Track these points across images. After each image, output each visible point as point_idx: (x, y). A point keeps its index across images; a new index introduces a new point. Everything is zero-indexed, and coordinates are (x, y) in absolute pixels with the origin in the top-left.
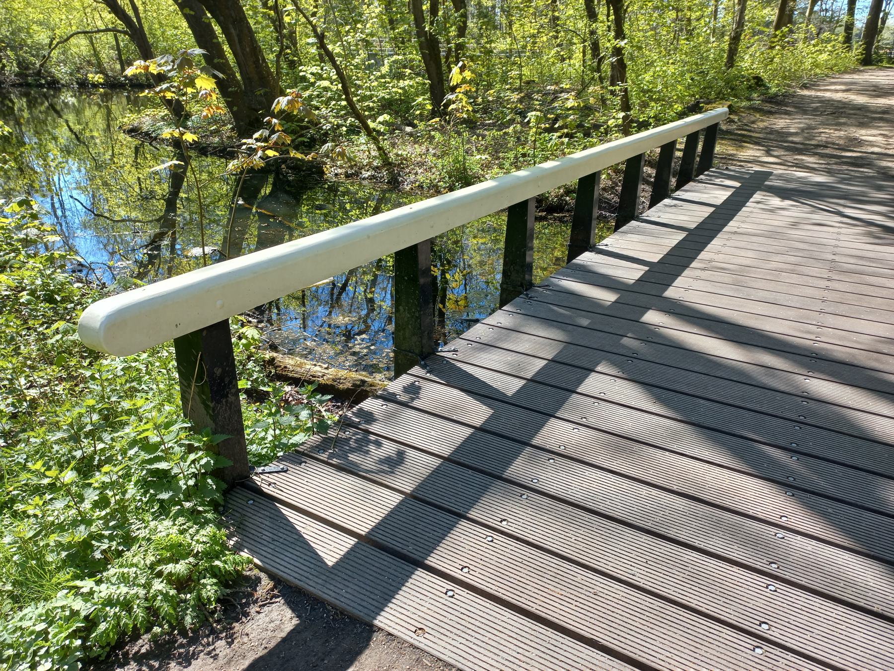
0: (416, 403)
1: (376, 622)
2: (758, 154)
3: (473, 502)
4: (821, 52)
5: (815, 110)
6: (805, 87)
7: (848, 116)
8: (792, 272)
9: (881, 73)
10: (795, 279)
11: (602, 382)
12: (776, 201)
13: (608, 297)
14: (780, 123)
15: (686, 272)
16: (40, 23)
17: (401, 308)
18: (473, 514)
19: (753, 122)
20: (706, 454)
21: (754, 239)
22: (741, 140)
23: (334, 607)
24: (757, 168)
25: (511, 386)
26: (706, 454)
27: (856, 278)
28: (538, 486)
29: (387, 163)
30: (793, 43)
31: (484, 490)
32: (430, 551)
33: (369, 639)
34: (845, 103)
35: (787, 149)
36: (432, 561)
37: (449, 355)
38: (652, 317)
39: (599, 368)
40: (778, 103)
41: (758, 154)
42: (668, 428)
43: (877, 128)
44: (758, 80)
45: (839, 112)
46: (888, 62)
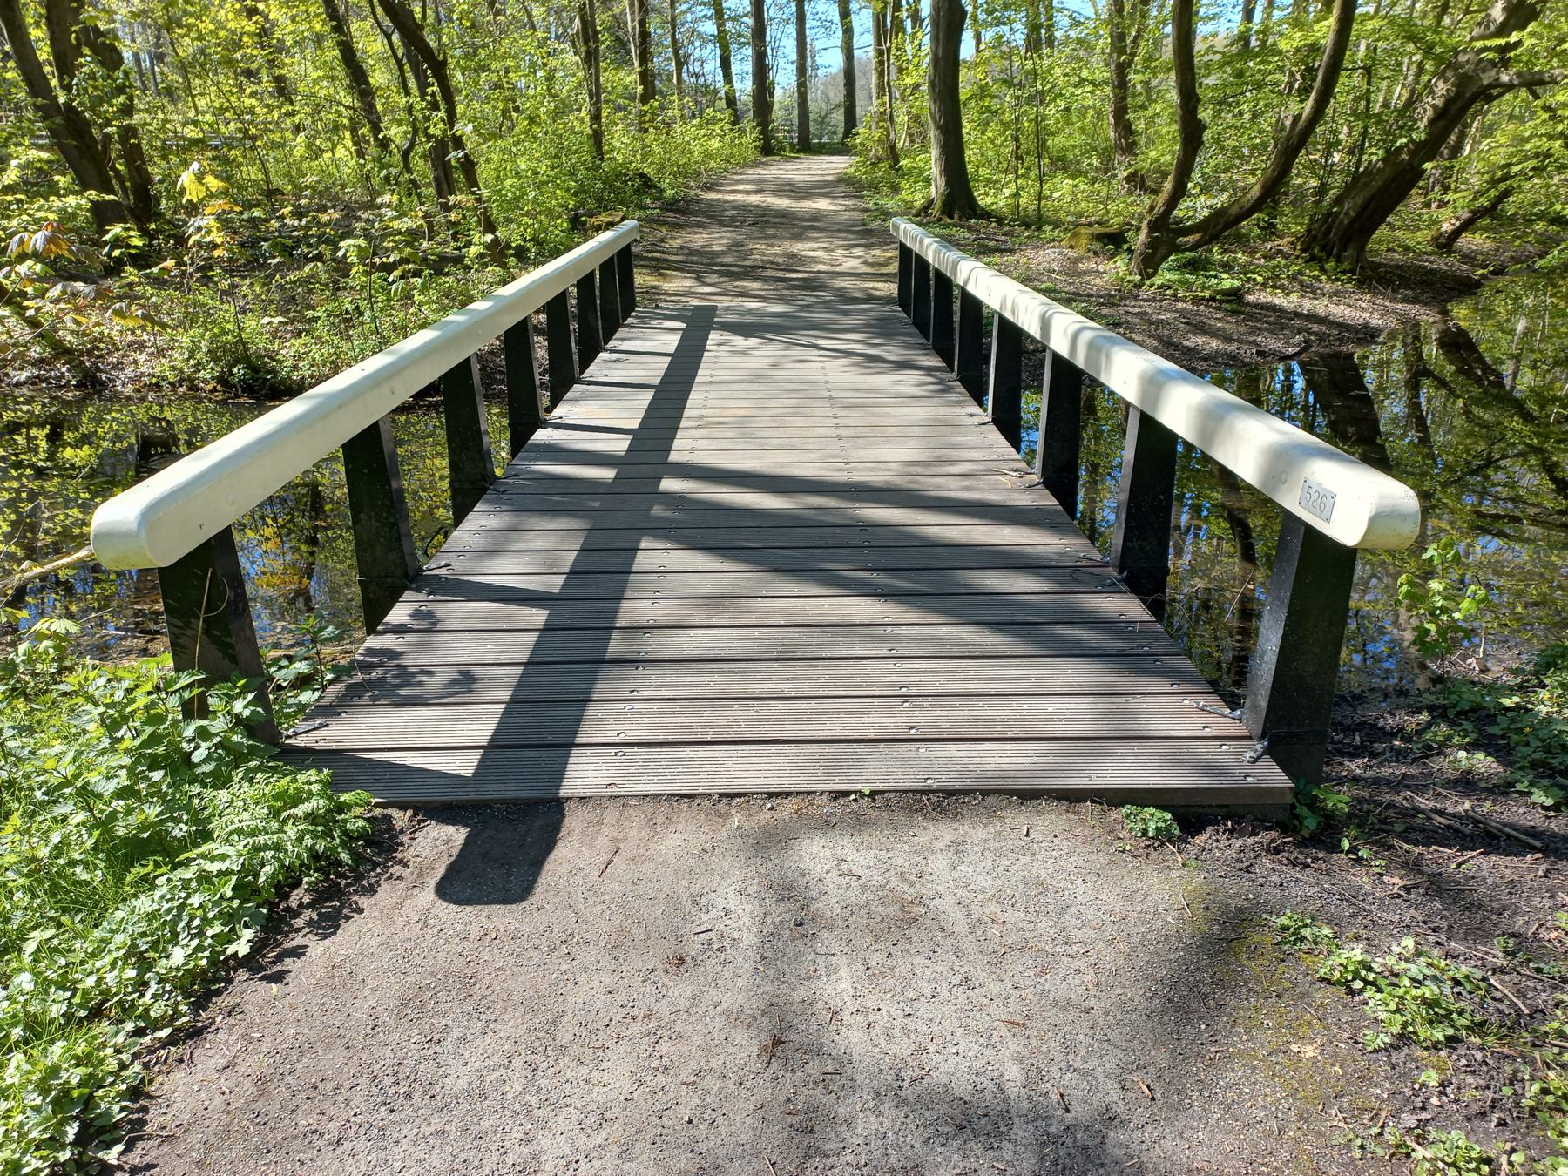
0: (439, 627)
1: (563, 793)
2: (688, 283)
3: (590, 687)
4: (710, 136)
5: (733, 219)
6: (707, 187)
7: (775, 226)
8: (795, 415)
9: (789, 166)
10: (800, 422)
11: (653, 556)
12: (739, 341)
13: (608, 474)
14: (699, 239)
15: (679, 434)
16: (1475, 199)
17: (362, 516)
18: (595, 696)
19: (662, 240)
20: (796, 591)
21: (736, 387)
22: (659, 267)
23: (502, 802)
24: (696, 302)
25: (556, 583)
26: (796, 591)
27: (860, 412)
28: (647, 657)
29: (61, 351)
30: (669, 125)
31: (594, 674)
32: (575, 733)
33: (562, 815)
34: (765, 209)
35: (721, 274)
36: (580, 739)
37: (443, 571)
38: (669, 484)
39: (642, 546)
40: (683, 212)
41: (688, 283)
42: (749, 580)
43: (815, 239)
44: (647, 183)
45: (762, 221)
46: (792, 151)
